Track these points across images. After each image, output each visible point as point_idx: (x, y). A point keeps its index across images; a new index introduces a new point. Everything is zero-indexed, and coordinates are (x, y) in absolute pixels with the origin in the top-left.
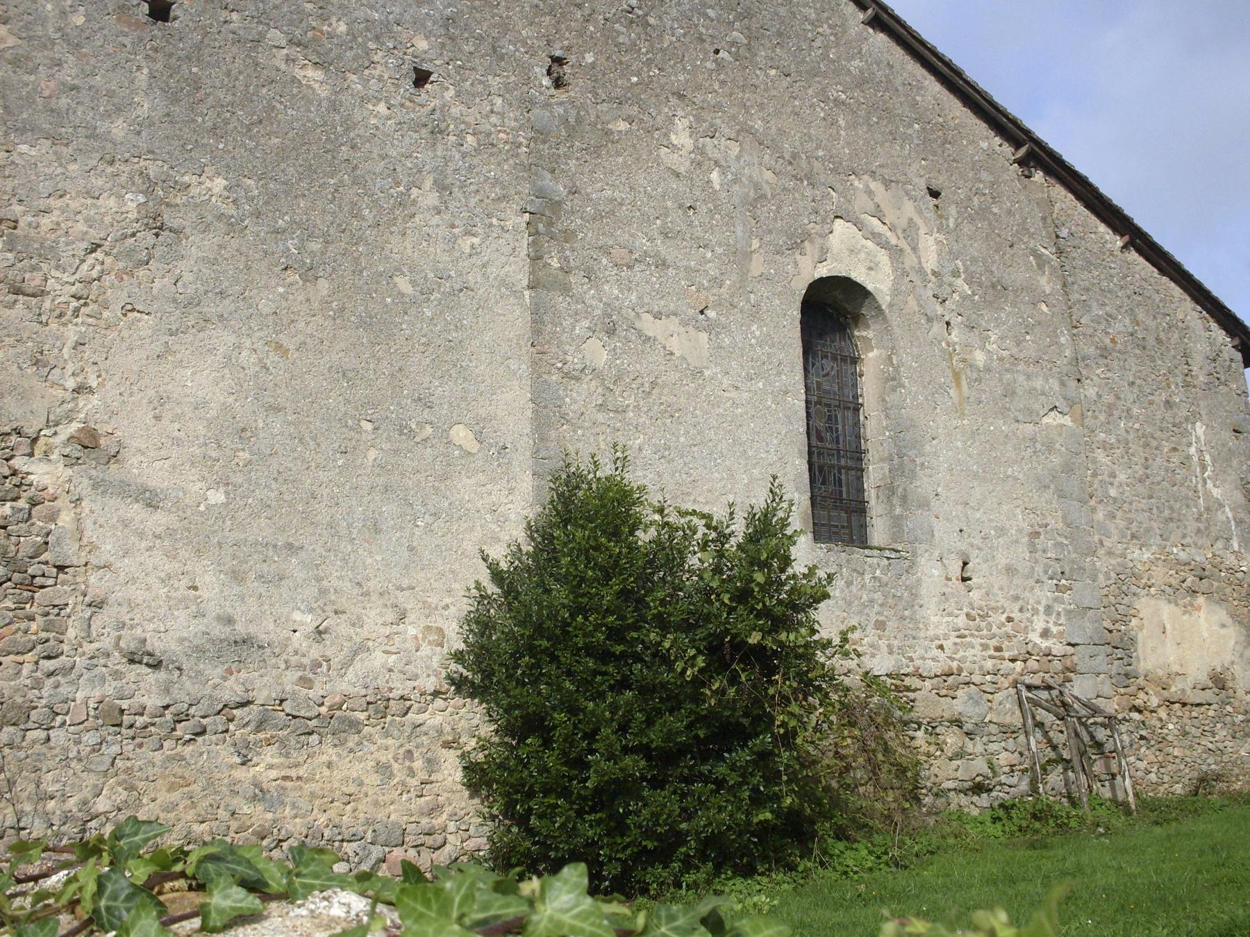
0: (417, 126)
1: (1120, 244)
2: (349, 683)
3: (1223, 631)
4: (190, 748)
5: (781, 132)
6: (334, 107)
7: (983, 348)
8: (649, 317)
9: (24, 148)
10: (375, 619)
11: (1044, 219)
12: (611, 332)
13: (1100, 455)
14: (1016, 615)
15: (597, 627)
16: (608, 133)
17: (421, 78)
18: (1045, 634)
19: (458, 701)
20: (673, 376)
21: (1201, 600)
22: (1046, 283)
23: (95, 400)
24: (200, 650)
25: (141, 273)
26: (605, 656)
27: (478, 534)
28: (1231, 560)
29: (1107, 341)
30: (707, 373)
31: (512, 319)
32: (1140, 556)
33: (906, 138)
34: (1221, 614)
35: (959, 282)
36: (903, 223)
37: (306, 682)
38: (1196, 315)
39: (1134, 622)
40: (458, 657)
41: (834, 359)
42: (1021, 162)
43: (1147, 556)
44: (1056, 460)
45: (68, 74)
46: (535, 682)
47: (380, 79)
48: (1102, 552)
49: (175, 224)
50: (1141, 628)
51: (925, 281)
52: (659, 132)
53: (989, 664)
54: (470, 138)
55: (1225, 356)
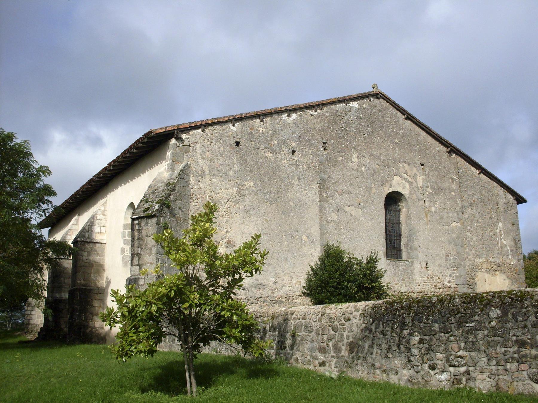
0: (293, 165)
1: (478, 172)
2: (281, 293)
3: (505, 281)
4: (250, 307)
5: (381, 154)
6: (275, 162)
7: (434, 207)
8: (346, 207)
9: (213, 180)
10: (287, 279)
11: (455, 168)
12: (338, 211)
13: (469, 234)
14: (441, 277)
15: (335, 282)
16: (337, 161)
17: (294, 152)
18: (449, 282)
19: (304, 297)
20: (352, 221)
21: (498, 273)
22: (454, 187)
23: (230, 234)
24: (252, 286)
25: (237, 205)
26: (336, 288)
27: (308, 260)
28: (508, 261)
29: (472, 201)
30: (361, 219)
31: (315, 209)
32: (479, 261)
33: (415, 150)
34: (504, 276)
35: (429, 189)
36: (413, 174)
37: (273, 293)
38: (501, 191)
39: (476, 279)
40: (304, 287)
41: (394, 211)
42: (449, 152)
43: (481, 260)
44: (454, 235)
45: (221, 162)
46: (322, 293)
47: (285, 154)
48: (467, 260)
49: (243, 194)
50: (478, 280)
51: (419, 190)
52: (349, 159)
53: (433, 290)
54: (305, 166)
55: (511, 202)
